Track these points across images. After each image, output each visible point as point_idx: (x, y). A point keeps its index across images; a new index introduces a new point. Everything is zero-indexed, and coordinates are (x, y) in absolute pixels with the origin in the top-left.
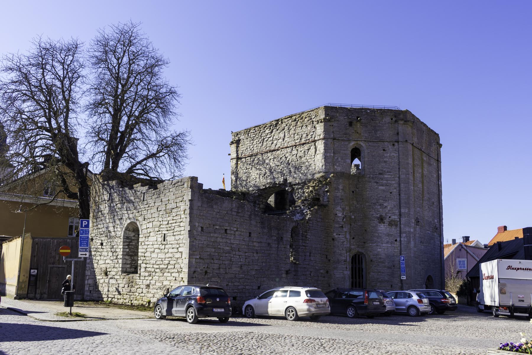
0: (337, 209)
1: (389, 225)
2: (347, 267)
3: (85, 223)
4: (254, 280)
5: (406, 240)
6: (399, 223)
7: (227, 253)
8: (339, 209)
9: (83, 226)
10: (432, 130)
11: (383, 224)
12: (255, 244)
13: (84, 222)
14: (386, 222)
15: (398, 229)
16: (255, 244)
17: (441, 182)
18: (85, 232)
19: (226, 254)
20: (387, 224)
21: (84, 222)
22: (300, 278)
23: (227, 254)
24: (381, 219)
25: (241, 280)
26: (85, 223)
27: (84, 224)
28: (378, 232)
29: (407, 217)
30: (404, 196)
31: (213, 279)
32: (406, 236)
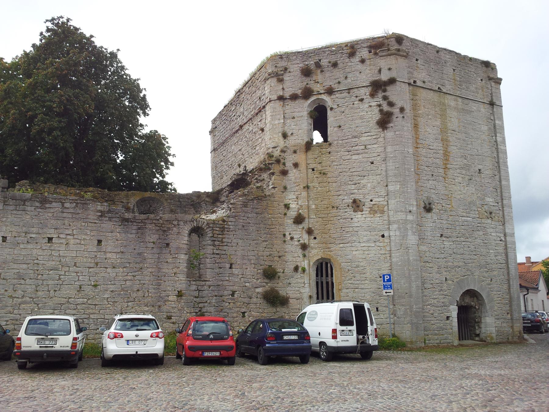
0: (290, 198)
1: (370, 212)
2: (306, 282)
3: (387, 277)
4: (109, 305)
5: (398, 233)
6: (386, 208)
7: (52, 270)
8: (292, 198)
9: (386, 281)
10: (428, 44)
11: (360, 213)
12: (109, 255)
13: (386, 276)
14: (365, 209)
15: (386, 218)
16: (109, 255)
17: (504, 139)
18: (386, 286)
19: (49, 271)
20: (367, 212)
21: (386, 276)
22: (209, 301)
23: (52, 271)
24: (356, 205)
25: (79, 307)
26: (387, 277)
27: (386, 279)
28: (353, 226)
29: (398, 198)
30: (392, 166)
31: (23, 306)
32: (399, 228)
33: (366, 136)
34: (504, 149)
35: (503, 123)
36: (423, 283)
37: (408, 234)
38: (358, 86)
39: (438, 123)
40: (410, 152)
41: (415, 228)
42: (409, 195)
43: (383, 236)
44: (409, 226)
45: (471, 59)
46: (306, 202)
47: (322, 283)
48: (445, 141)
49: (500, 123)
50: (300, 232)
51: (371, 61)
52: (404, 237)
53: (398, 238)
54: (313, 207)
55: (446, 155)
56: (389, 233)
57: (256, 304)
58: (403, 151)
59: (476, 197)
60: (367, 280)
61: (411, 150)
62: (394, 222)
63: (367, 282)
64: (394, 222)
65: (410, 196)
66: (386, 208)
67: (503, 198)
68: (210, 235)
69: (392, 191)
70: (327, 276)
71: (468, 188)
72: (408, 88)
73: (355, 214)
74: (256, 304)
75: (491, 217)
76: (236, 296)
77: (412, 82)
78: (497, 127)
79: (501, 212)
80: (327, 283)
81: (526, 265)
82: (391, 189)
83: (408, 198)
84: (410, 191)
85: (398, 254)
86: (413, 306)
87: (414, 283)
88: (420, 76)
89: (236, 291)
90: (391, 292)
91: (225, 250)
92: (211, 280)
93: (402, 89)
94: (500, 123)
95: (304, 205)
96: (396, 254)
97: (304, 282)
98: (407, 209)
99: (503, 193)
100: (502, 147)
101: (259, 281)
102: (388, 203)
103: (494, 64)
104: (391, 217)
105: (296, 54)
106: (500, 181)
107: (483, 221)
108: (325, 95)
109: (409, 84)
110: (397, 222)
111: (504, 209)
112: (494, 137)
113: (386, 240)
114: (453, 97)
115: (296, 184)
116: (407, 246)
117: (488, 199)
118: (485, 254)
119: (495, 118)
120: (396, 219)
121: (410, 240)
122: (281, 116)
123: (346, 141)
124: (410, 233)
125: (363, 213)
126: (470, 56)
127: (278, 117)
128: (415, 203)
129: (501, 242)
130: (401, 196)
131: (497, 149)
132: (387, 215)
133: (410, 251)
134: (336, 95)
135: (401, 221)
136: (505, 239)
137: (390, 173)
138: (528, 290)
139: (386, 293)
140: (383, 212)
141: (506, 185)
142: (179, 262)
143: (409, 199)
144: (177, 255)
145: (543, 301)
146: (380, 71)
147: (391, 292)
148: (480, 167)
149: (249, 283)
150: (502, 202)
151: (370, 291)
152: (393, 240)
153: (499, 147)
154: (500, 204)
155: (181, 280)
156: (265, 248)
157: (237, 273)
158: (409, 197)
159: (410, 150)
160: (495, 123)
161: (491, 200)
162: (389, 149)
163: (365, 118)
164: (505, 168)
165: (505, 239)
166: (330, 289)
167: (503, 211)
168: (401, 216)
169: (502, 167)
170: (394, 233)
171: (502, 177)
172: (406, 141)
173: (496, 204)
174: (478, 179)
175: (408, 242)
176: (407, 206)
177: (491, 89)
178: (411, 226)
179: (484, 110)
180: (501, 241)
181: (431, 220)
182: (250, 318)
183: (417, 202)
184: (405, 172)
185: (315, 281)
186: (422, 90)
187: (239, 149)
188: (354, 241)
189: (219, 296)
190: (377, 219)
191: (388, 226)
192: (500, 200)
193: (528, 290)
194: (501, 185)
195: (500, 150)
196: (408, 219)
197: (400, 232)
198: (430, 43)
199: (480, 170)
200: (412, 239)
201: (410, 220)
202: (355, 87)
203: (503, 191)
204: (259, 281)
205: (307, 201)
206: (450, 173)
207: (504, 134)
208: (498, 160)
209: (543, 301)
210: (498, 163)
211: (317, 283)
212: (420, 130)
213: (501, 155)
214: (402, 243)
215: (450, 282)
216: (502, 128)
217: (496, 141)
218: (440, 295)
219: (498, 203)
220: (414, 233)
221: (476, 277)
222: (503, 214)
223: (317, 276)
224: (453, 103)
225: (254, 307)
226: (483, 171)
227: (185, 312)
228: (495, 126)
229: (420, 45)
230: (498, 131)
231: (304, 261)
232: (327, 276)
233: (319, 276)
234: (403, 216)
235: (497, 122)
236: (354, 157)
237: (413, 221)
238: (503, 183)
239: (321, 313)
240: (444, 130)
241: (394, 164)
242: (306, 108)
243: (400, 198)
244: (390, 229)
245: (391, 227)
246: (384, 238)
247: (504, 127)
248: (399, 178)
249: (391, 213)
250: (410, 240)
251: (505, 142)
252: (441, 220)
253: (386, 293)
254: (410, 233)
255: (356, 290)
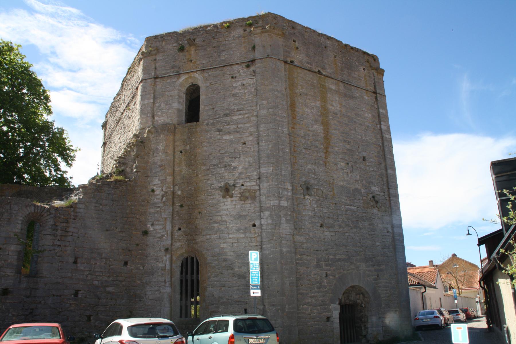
2: (167, 280)
5: (270, 221)
6: (258, 193)
10: (307, 28)
15: (257, 204)
22: (43, 302)
24: (227, 191)
29: (271, 181)
32: (271, 216)
33: (238, 114)
34: (390, 137)
35: (387, 112)
36: (298, 279)
37: (281, 222)
38: (231, 64)
39: (318, 104)
40: (285, 131)
41: (290, 215)
42: (283, 178)
43: (254, 225)
44: (282, 213)
45: (352, 48)
46: (171, 188)
47: (186, 281)
48: (326, 124)
49: (384, 112)
50: (163, 222)
51: (245, 39)
52: (277, 225)
53: (270, 227)
54: (179, 193)
55: (327, 138)
56: (261, 222)
57: (105, 306)
58: (277, 130)
59: (361, 185)
60: (235, 277)
61: (286, 130)
62: (267, 209)
63: (235, 279)
64: (267, 209)
65: (284, 180)
66: (258, 193)
67: (390, 187)
68: (51, 223)
69: (264, 173)
70: (192, 273)
71: (351, 174)
72: (283, 66)
73: (225, 200)
74: (105, 306)
75: (376, 207)
76: (80, 296)
77: (289, 60)
78: (381, 116)
79: (388, 203)
80: (192, 281)
81: (429, 268)
82: (264, 172)
83: (281, 181)
84: (284, 173)
85: (269, 246)
86: (286, 306)
87: (288, 279)
88: (298, 57)
89: (80, 291)
90: (258, 293)
91: (69, 242)
92: (48, 276)
93: (277, 67)
94: (384, 112)
95: (169, 191)
96: (267, 246)
97: (165, 280)
98: (281, 193)
99: (390, 183)
100: (387, 136)
101: (111, 279)
102: (260, 187)
103: (376, 56)
104: (263, 203)
105: (171, 34)
106: (386, 170)
107: (369, 210)
108: (197, 74)
109: (286, 62)
110: (269, 209)
111: (391, 198)
112: (378, 126)
113: (257, 230)
114: (334, 81)
115: (161, 168)
116: (280, 236)
117: (374, 187)
118: (371, 246)
119: (379, 107)
120: (268, 205)
121: (284, 229)
122: (151, 95)
123: (217, 120)
124: (283, 220)
125: (234, 198)
126: (352, 45)
127: (148, 96)
128: (290, 188)
129: (388, 234)
130: (274, 180)
131: (382, 138)
132: (258, 201)
133: (283, 242)
134: (209, 73)
135: (273, 207)
136: (393, 230)
137: (263, 154)
138: (425, 288)
139: (253, 293)
140: (254, 198)
141: (392, 174)
142: (7, 253)
143: (282, 183)
144: (5, 246)
145: (440, 299)
146: (254, 48)
147: (258, 293)
148: (364, 154)
149: (98, 281)
150: (389, 191)
151: (238, 290)
152: (264, 230)
153: (384, 135)
154: (386, 193)
155: (9, 276)
156: (121, 240)
157: (82, 268)
158: (283, 180)
159: (285, 129)
160: (379, 111)
161: (377, 189)
162: (262, 127)
163: (238, 95)
164: (391, 157)
165: (393, 230)
166: (195, 288)
167: (390, 200)
168: (273, 202)
169: (388, 156)
170: (266, 221)
171: (388, 166)
172: (281, 119)
173: (383, 194)
174: (363, 167)
175: (280, 231)
176: (281, 191)
177: (374, 79)
178: (285, 213)
179: (368, 98)
180: (388, 232)
181: (309, 207)
182: (98, 322)
183: (292, 186)
184: (279, 153)
185: (179, 279)
186: (299, 70)
187: (118, 138)
188: (222, 232)
189: (57, 296)
190: (249, 206)
191: (259, 213)
192: (387, 190)
193: (425, 288)
194: (387, 174)
195: (384, 138)
196: (281, 205)
197: (272, 219)
198: (309, 27)
199: (364, 157)
200: (286, 228)
201: (283, 206)
202: (229, 64)
203: (389, 180)
204: (111, 279)
205: (172, 187)
206: (331, 158)
207: (388, 123)
208: (383, 148)
209: (440, 299)
210: (384, 150)
211: (181, 281)
212: (297, 109)
213: (386, 144)
214: (274, 232)
215: (331, 277)
216: (387, 117)
217: (381, 129)
218: (319, 292)
219: (384, 192)
220: (288, 221)
221: (361, 272)
222: (390, 204)
223: (182, 273)
224: (333, 87)
225: (103, 309)
226: (368, 158)
227: (10, 315)
228: (379, 115)
229: (299, 27)
230: (382, 119)
231: (166, 256)
232: (192, 273)
233: (184, 274)
234: (276, 201)
235: (381, 110)
236: (226, 137)
237: (287, 207)
238: (389, 171)
239: (181, 317)
240: (324, 112)
241: (267, 144)
242: (177, 87)
243: (272, 181)
244: (262, 217)
245: (262, 215)
246: (254, 228)
247: (388, 116)
248: (272, 159)
249: (263, 198)
250: (284, 229)
251: (390, 131)
252: (321, 209)
253: (253, 293)
254: (283, 220)
255: (223, 289)
